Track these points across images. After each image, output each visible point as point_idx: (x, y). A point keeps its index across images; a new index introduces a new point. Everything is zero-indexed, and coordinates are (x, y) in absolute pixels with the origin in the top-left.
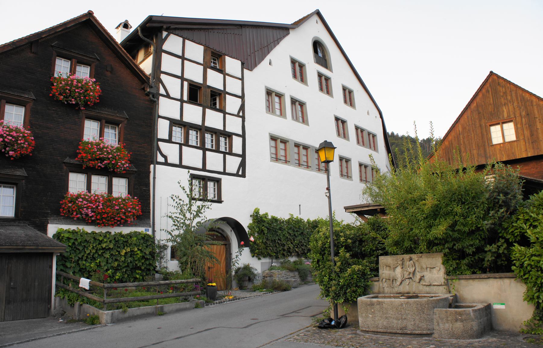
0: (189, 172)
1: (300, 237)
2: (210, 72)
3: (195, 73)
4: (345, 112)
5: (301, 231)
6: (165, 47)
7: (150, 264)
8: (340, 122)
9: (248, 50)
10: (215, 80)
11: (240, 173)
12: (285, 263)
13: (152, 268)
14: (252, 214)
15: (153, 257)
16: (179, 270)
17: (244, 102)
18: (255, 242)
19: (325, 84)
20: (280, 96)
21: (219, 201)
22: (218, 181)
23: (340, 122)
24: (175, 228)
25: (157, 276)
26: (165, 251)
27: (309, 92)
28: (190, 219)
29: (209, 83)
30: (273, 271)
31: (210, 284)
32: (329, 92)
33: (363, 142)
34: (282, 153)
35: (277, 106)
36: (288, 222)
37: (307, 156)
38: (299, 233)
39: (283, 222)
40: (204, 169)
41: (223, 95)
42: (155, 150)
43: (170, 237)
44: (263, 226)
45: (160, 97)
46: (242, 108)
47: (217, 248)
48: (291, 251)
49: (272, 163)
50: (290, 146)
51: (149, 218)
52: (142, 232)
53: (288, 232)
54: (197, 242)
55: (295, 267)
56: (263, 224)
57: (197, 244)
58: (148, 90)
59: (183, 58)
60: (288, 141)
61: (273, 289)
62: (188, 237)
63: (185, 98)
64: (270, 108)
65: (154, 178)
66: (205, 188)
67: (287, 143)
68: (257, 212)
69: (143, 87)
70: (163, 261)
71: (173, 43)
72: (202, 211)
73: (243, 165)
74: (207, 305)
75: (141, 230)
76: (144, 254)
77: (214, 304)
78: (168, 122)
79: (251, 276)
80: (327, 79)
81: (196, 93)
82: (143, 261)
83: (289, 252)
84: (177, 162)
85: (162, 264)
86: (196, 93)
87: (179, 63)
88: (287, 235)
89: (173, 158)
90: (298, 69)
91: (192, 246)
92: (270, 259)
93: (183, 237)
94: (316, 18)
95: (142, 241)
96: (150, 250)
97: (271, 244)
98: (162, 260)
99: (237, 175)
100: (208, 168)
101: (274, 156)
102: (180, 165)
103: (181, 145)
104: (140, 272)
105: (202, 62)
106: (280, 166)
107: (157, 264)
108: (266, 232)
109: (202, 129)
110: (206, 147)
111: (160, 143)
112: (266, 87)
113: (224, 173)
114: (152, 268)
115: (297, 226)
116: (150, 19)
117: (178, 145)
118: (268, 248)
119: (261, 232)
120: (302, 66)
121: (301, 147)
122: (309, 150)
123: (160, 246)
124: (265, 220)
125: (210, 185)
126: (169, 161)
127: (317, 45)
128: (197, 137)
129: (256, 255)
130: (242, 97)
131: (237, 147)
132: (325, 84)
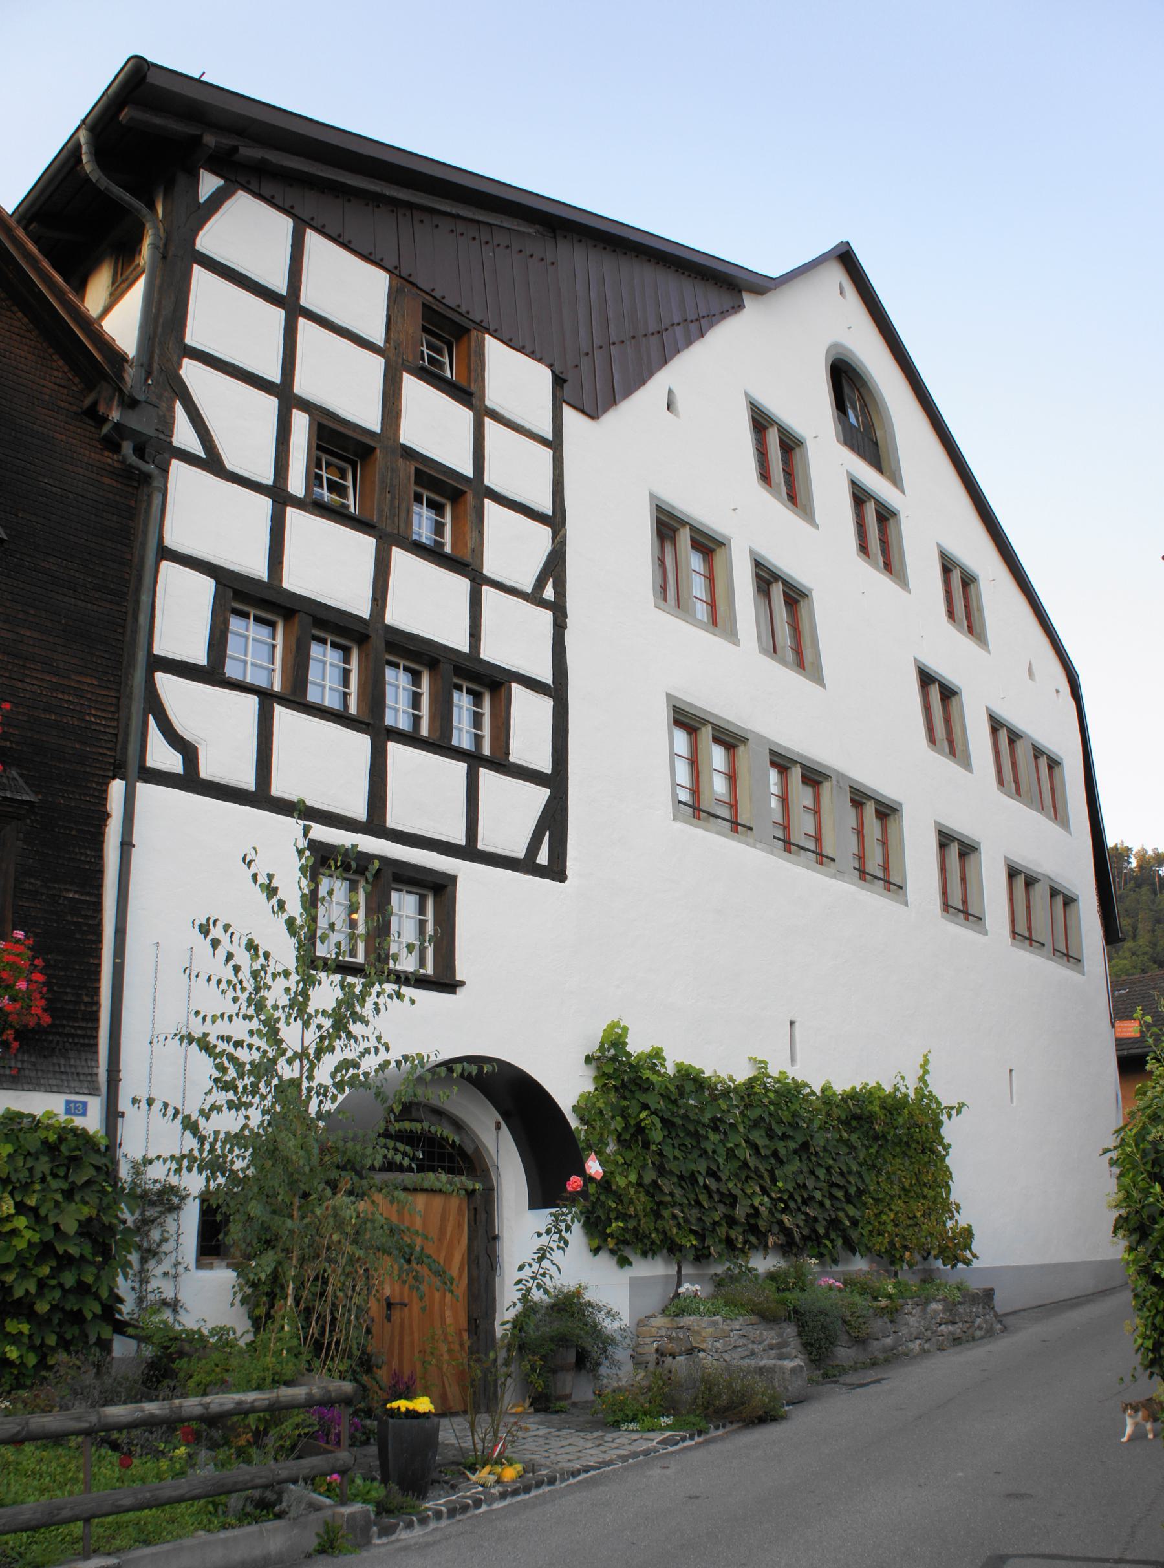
0: (306, 830)
1: (794, 1166)
2: (413, 388)
3: (347, 384)
4: (952, 655)
5: (800, 1139)
6: (208, 240)
7: (83, 1289)
8: (935, 691)
9: (582, 331)
10: (433, 426)
11: (543, 858)
12: (733, 1279)
13: (92, 1308)
14: (593, 1048)
15: (104, 1250)
16: (238, 1323)
18: (605, 1184)
19: (877, 529)
20: (708, 545)
21: (445, 981)
22: (439, 889)
23: (937, 691)
24: (222, 1097)
25: (122, 1347)
26: (170, 1223)
27: (819, 550)
28: (302, 1055)
29: (408, 436)
30: (687, 1320)
31: (403, 1404)
32: (890, 562)
33: (1017, 782)
34: (719, 785)
35: (698, 587)
36: (749, 1092)
37: (817, 812)
38: (792, 1145)
39: (726, 1093)
40: (375, 824)
41: (470, 498)
42: (137, 706)
43: (191, 1143)
44: (645, 1107)
45: (175, 462)
46: (555, 566)
47: (427, 1211)
48: (762, 1225)
49: (679, 825)
50: (751, 759)
51: (93, 1047)
52: (50, 1115)
53: (747, 1141)
54: (334, 1174)
55: (784, 1302)
56: (643, 1098)
57: (333, 1186)
58: (115, 415)
59: (290, 305)
60: (744, 740)
61: (707, 1418)
62: (290, 1144)
63: (296, 485)
64: (668, 590)
65: (127, 845)
66: (379, 908)
67: (741, 750)
68: (615, 1041)
69: (88, 402)
70: (157, 1269)
71: (246, 230)
72: (367, 1010)
73: (554, 821)
74: (386, 1531)
75: (43, 1104)
76: (50, 1235)
77: (423, 1521)
78: (207, 585)
79: (588, 1343)
80: (886, 515)
81: (353, 469)
82: (45, 1270)
83: (753, 1229)
84: (247, 780)
85: (154, 1284)
86: (353, 469)
87: (266, 325)
88: (747, 1154)
89: (228, 757)
90: (778, 453)
91: (305, 1195)
92: (667, 1262)
93: (265, 1149)
94: (836, 275)
95: (43, 1165)
96: (86, 1211)
97: (678, 1192)
98: (152, 1263)
99: (526, 865)
101: (684, 796)
102: (260, 797)
103: (267, 698)
104: (25, 1328)
105: (379, 339)
107: (123, 1286)
108: (657, 1135)
109: (371, 641)
110: (389, 720)
111: (165, 682)
113: (470, 851)
114: (92, 1308)
115: (785, 1115)
117: (253, 700)
118: (666, 1213)
119: (634, 1137)
120: (791, 445)
121: (796, 774)
122: (826, 788)
123: (145, 1194)
124: (654, 1078)
125: (403, 904)
126: (208, 770)
127: (845, 378)
128: (346, 673)
129: (611, 1243)
130: (556, 521)
131: (530, 743)
132: (877, 529)
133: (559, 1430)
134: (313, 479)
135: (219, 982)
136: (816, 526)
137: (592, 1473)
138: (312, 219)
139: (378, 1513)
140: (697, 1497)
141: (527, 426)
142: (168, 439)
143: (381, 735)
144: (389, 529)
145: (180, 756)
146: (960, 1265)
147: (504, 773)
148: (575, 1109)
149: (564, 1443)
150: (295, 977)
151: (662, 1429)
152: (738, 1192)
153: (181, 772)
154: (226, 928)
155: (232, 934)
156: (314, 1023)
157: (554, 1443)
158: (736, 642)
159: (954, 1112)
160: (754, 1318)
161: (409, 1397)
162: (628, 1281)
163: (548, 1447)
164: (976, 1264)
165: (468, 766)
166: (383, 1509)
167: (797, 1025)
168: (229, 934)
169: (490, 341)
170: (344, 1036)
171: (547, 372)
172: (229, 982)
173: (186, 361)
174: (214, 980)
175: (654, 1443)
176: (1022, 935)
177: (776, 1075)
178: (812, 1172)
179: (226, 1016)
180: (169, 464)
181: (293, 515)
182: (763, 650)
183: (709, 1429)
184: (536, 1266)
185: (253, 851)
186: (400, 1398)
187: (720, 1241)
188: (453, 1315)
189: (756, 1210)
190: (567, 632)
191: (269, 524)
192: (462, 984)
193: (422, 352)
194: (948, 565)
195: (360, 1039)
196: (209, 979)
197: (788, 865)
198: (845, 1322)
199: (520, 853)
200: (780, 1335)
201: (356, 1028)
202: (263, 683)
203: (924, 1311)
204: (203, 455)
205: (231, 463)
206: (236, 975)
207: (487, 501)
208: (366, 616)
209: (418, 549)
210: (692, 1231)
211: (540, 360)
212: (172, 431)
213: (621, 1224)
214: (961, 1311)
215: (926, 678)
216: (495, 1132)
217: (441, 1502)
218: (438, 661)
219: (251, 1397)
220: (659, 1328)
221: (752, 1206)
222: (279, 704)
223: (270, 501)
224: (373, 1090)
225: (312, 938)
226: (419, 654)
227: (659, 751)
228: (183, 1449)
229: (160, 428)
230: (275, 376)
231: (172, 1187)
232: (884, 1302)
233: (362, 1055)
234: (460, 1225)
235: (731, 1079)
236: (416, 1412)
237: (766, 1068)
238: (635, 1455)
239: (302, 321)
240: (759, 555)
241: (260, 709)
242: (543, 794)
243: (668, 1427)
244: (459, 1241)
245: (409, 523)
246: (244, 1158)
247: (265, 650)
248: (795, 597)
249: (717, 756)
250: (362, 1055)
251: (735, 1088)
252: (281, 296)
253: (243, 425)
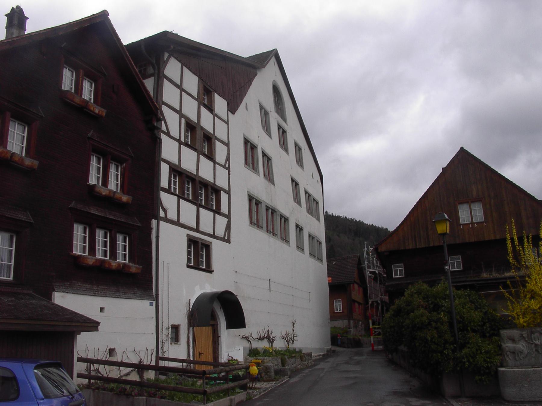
11: (226, 238)
65: (158, 237)
73: (228, 227)
87: (178, 93)
89: (172, 215)
99: (223, 239)
112: (244, 135)
113: (213, 236)
116: (165, 34)
126: (169, 217)
127: (276, 90)
131: (224, 209)
176: (312, 255)
194: (296, 145)
215: (293, 180)
226: (205, 184)
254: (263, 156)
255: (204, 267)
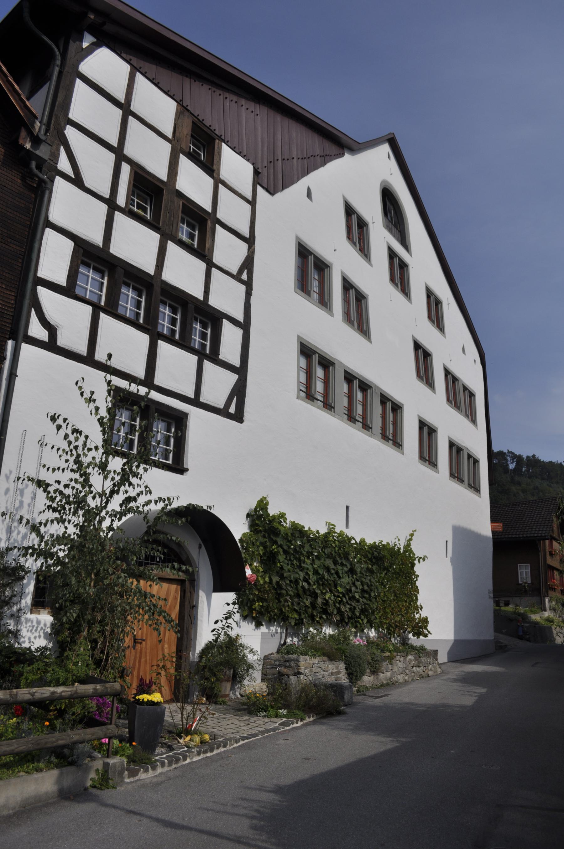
2: (184, 162)
6: (85, 67)
10: (192, 183)
11: (232, 410)
17: (253, 253)
19: (399, 273)
22: (178, 421)
27: (372, 277)
31: (145, 697)
32: (405, 289)
34: (319, 387)
39: (315, 539)
40: (148, 381)
42: (27, 302)
46: (248, 264)
49: (300, 402)
59: (126, 108)
63: (121, 200)
64: (303, 286)
66: (146, 431)
73: (239, 392)
78: (69, 245)
80: (403, 266)
81: (151, 198)
86: (151, 198)
89: (74, 336)
90: (356, 229)
99: (223, 412)
100: (158, 380)
102: (89, 359)
103: (97, 309)
106: (315, 413)
109: (152, 288)
110: (159, 329)
111: (42, 291)
113: (196, 402)
119: (269, 560)
120: (362, 225)
125: (159, 428)
126: (61, 342)
127: (388, 197)
130: (250, 241)
132: (399, 273)
133: (224, 714)
134: (129, 201)
135: (58, 449)
136: (371, 265)
137: (246, 741)
138: (140, 68)
139: (128, 762)
140: (309, 759)
141: (240, 192)
142: (55, 165)
143: (155, 336)
144: (167, 231)
145: (47, 332)
146: (421, 637)
147: (216, 364)
148: (241, 540)
149: (229, 722)
150: (101, 451)
151: (281, 717)
152: (318, 591)
153: (47, 341)
154: (65, 420)
155: (68, 424)
156: (110, 476)
157: (224, 723)
158: (332, 315)
159: (421, 560)
160: (325, 658)
161: (149, 693)
162: (260, 634)
163: (220, 724)
164: (430, 637)
165: (199, 358)
166: (132, 760)
167: (350, 508)
168: (66, 424)
169: (225, 147)
170: (127, 484)
171: (251, 167)
172: (64, 450)
173: (68, 127)
174: (56, 448)
175: (277, 725)
177: (339, 532)
178: (354, 584)
179: (61, 469)
180: (55, 178)
181: (118, 216)
182: (344, 320)
183: (305, 717)
184: (224, 621)
185: (82, 380)
186: (144, 693)
187: (308, 616)
188: (169, 648)
189: (327, 601)
190: (252, 297)
191: (105, 218)
192: (187, 470)
193: (190, 147)
194: (429, 294)
195: (136, 486)
196: (53, 447)
197: (349, 427)
198: (370, 663)
199: (221, 406)
200: (337, 668)
201: (134, 480)
202: (95, 299)
203: (405, 659)
204: (73, 177)
205: (88, 183)
206: (69, 446)
207: (217, 225)
208: (152, 273)
209: (181, 243)
210: (295, 610)
211: (248, 160)
212: (58, 161)
213: (261, 604)
214: (423, 660)
215: (417, 346)
216: (198, 549)
217: (164, 756)
218: (187, 303)
219: (60, 690)
220: (275, 661)
221: (325, 599)
222: (103, 312)
223: (107, 207)
224: (143, 515)
225: (111, 428)
226: (178, 298)
227: (291, 366)
228: (15, 719)
229: (51, 158)
230: (114, 142)
231: (21, 566)
232: (387, 654)
233: (138, 495)
234: (175, 598)
235: (318, 532)
236: (153, 702)
237: (334, 529)
238: (268, 731)
239: (131, 118)
240: (345, 275)
241: (92, 314)
242: (234, 377)
243: (284, 716)
244: (175, 607)
245: (177, 231)
246: (64, 551)
247: (97, 284)
248: (361, 298)
249: (320, 372)
250: (138, 495)
251: (319, 537)
252: (121, 103)
253: (97, 167)
254: (464, 391)
255: (170, 462)
